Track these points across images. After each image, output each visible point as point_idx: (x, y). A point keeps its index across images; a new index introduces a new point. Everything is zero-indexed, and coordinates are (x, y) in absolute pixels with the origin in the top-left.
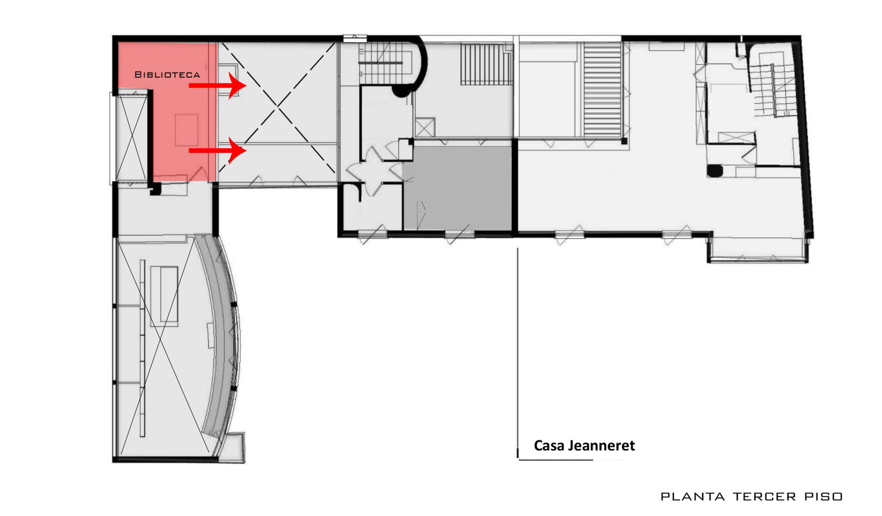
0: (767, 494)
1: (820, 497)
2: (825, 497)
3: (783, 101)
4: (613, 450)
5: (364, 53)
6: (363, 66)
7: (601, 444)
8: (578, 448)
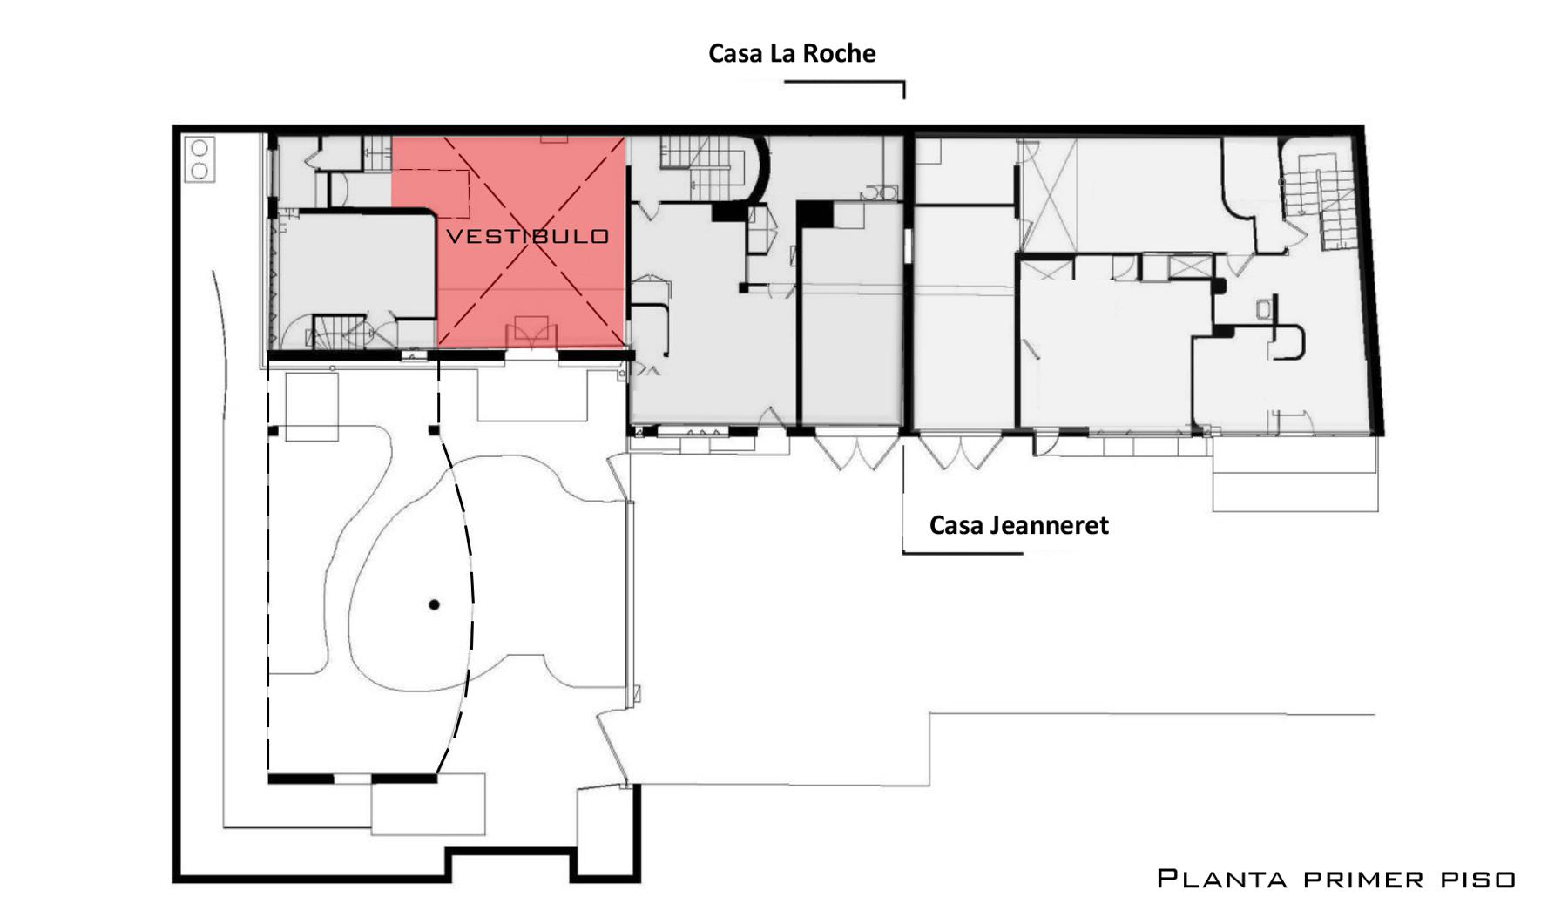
0: (1511, 884)
1: (1470, 881)
2: (1481, 879)
4: (1071, 533)
7: (1049, 523)
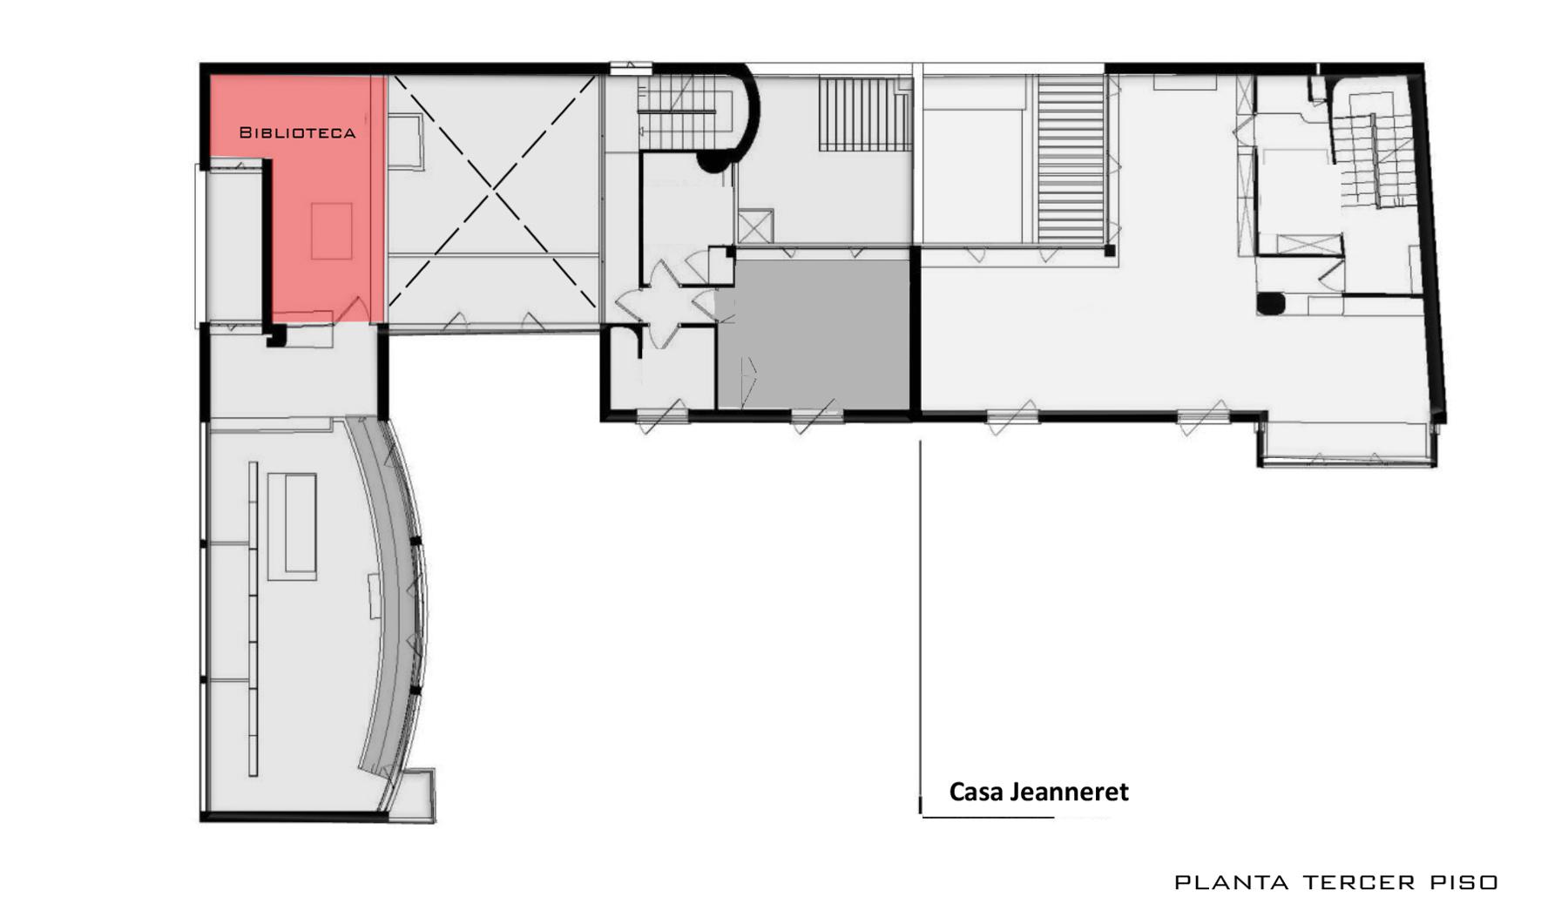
0: (1364, 879)
1: (1457, 883)
2: (1467, 883)
3: (1392, 179)
4: (1091, 799)
5: (647, 94)
6: (645, 117)
7: (1068, 790)
8: (1027, 796)
